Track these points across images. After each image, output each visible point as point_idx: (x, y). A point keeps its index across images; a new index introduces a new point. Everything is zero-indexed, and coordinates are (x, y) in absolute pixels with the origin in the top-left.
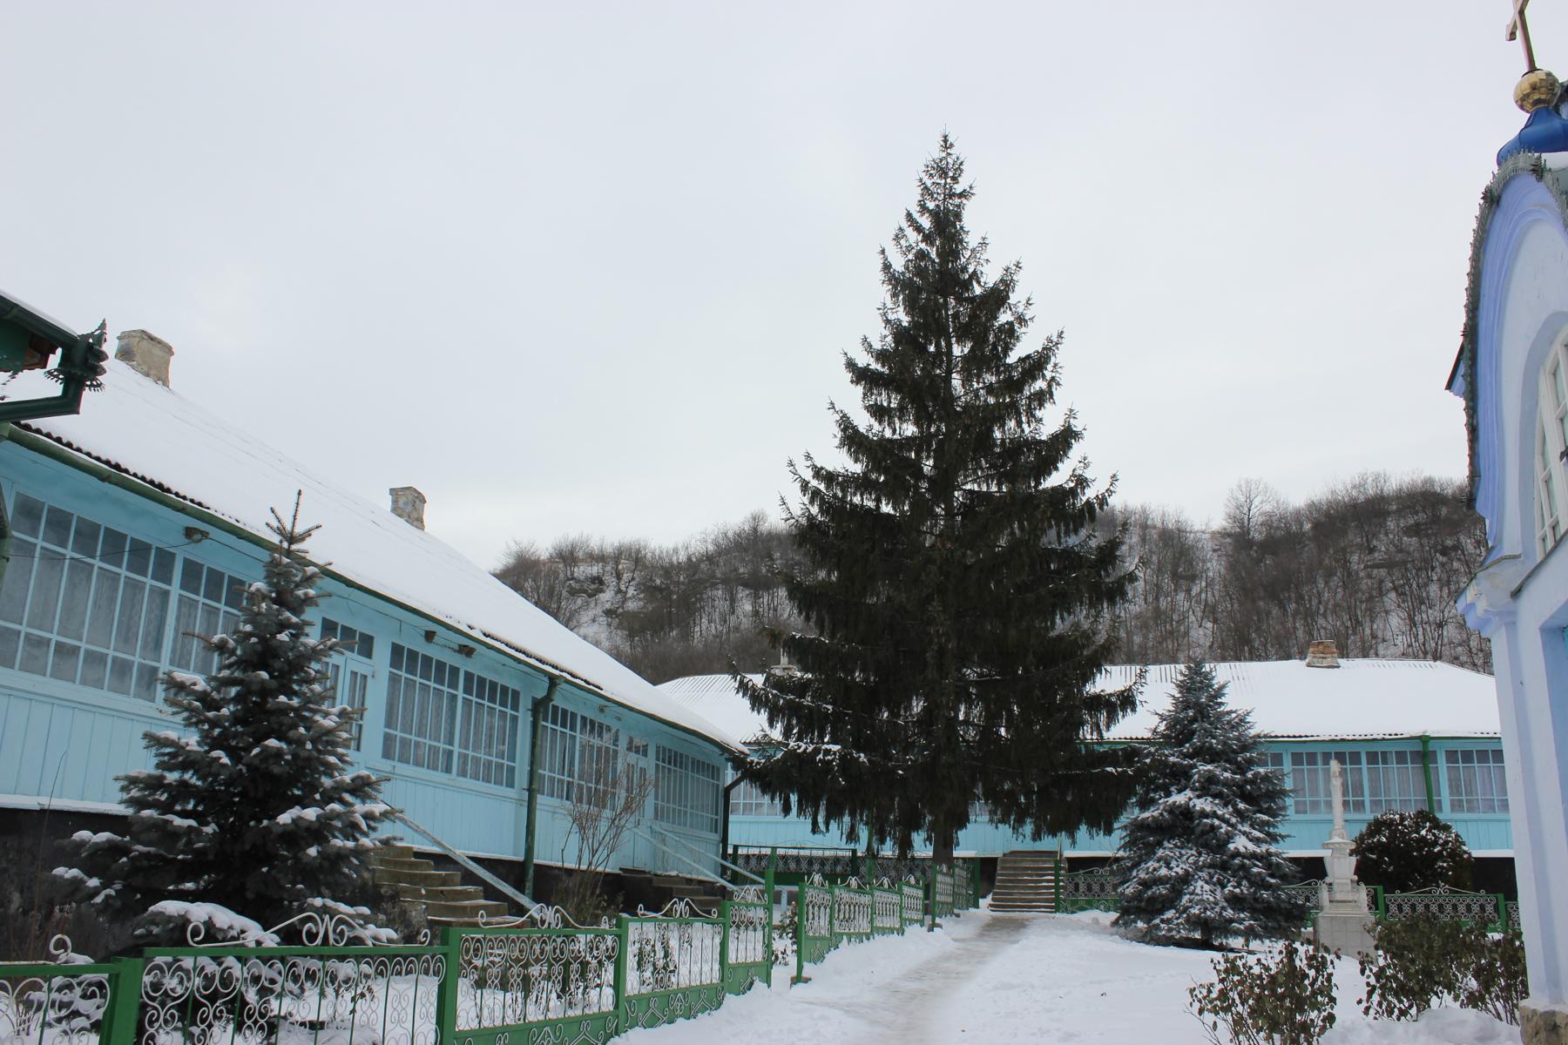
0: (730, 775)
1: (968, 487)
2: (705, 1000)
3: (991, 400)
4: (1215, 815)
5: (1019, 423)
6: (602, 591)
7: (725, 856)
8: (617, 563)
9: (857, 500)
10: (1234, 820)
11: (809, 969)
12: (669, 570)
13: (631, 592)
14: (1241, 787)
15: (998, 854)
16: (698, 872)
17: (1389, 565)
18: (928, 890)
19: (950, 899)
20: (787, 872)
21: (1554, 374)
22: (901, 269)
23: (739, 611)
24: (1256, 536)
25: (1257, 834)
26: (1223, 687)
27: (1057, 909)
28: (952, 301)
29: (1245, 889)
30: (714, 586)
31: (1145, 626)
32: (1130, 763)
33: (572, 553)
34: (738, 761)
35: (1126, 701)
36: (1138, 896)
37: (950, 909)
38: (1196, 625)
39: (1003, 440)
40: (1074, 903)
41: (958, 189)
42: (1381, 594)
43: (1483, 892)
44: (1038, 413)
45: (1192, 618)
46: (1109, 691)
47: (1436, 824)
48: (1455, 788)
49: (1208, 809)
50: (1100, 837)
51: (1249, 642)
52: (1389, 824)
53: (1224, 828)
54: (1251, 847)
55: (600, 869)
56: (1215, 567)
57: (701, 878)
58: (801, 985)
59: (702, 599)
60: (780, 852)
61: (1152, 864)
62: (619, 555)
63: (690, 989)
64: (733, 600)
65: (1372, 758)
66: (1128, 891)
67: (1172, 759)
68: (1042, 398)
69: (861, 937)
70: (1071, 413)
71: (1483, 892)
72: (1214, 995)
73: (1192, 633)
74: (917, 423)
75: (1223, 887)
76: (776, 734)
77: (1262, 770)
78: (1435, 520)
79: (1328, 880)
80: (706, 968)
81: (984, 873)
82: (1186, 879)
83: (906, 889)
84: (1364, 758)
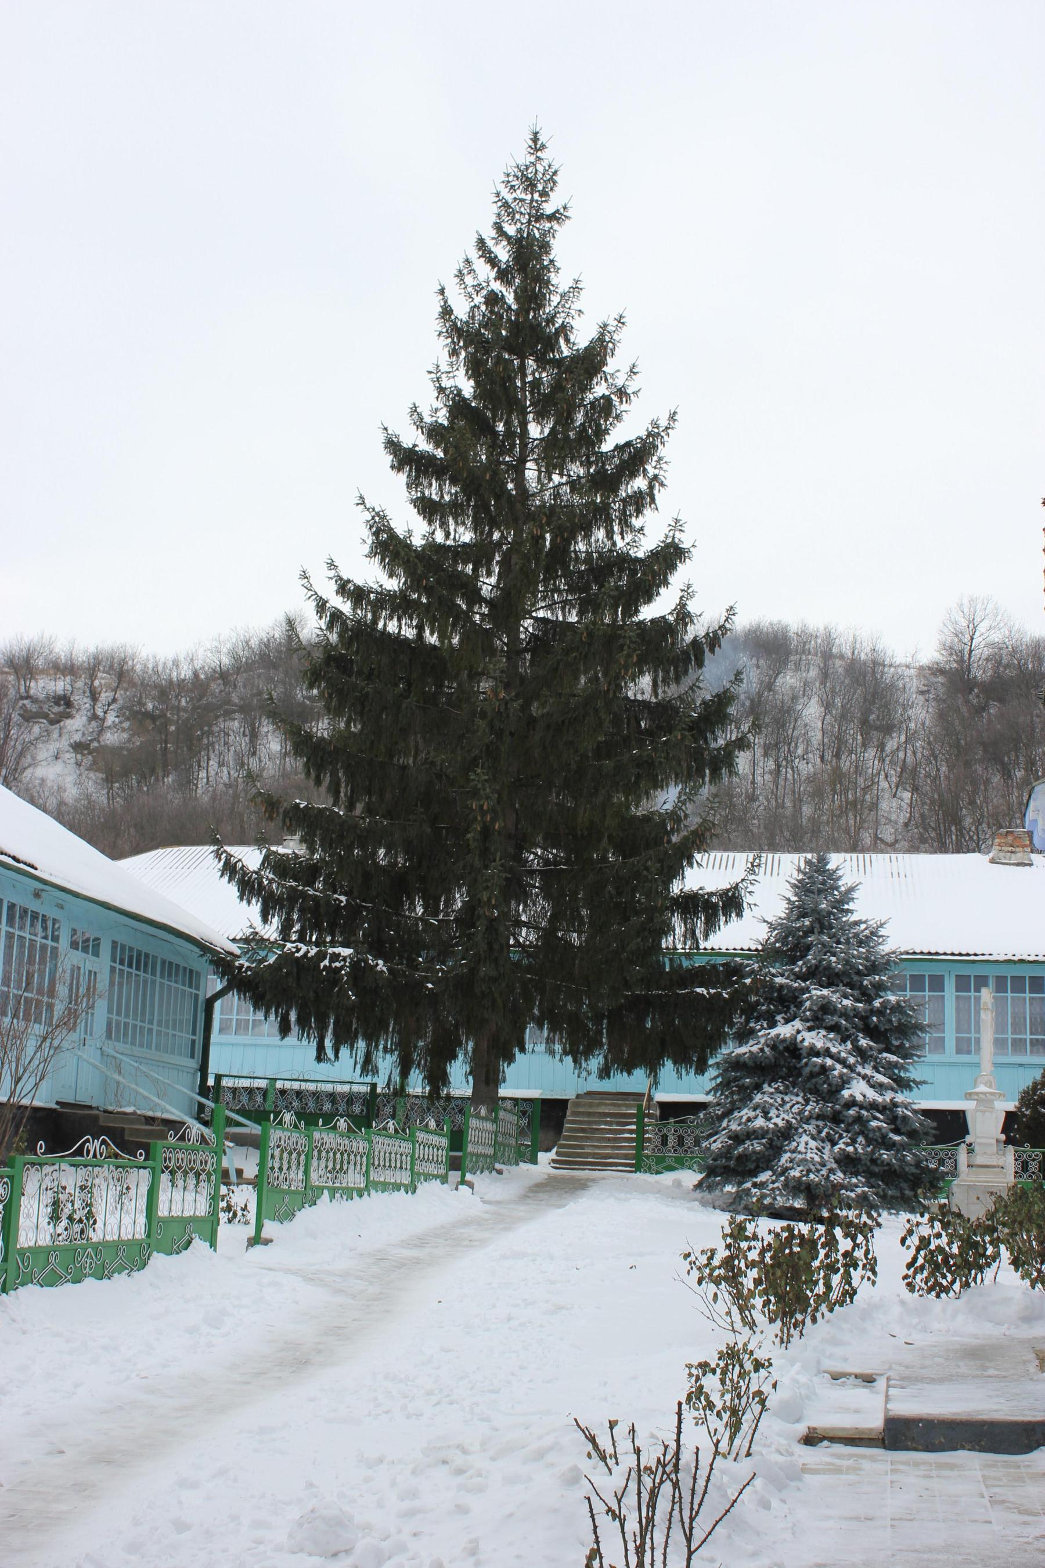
0: (215, 983)
1: (541, 614)
2: (131, 1257)
3: (576, 499)
4: (827, 1053)
5: (610, 534)
6: (69, 716)
7: (204, 1090)
8: (92, 677)
9: (392, 627)
10: (852, 1060)
11: (270, 1228)
12: (166, 689)
13: (111, 718)
14: (865, 1019)
15: (569, 1094)
16: (167, 1111)
18: (457, 1140)
19: (491, 1151)
20: (261, 1106)
22: (465, 318)
23: (262, 751)
24: (978, 673)
25: (881, 1078)
26: (852, 889)
27: (637, 1168)
28: (531, 363)
29: (861, 1147)
30: (228, 715)
31: (818, 794)
32: (726, 983)
33: (27, 660)
34: (223, 963)
35: (731, 902)
36: (726, 1153)
37: (489, 1164)
38: (887, 795)
39: (589, 554)
40: (660, 1160)
41: (548, 208)
44: (636, 522)
45: (884, 784)
46: (709, 889)
49: (819, 1045)
50: (691, 1078)
51: (957, 821)
54: (872, 1095)
55: (25, 1102)
56: (921, 714)
57: (166, 1116)
58: (258, 1248)
59: (210, 733)
60: (279, 1085)
61: (746, 1113)
62: (94, 667)
63: (104, 1244)
64: (254, 736)
65: (1001, 984)
66: (714, 1147)
67: (779, 980)
68: (640, 502)
69: (349, 1193)
70: (677, 525)
72: (716, 1262)
73: (884, 805)
74: (476, 527)
75: (834, 1143)
76: (271, 931)
77: (892, 998)
79: (968, 1139)
80: (127, 1220)
81: (548, 1117)
82: (787, 1133)
83: (421, 1136)
84: (991, 982)
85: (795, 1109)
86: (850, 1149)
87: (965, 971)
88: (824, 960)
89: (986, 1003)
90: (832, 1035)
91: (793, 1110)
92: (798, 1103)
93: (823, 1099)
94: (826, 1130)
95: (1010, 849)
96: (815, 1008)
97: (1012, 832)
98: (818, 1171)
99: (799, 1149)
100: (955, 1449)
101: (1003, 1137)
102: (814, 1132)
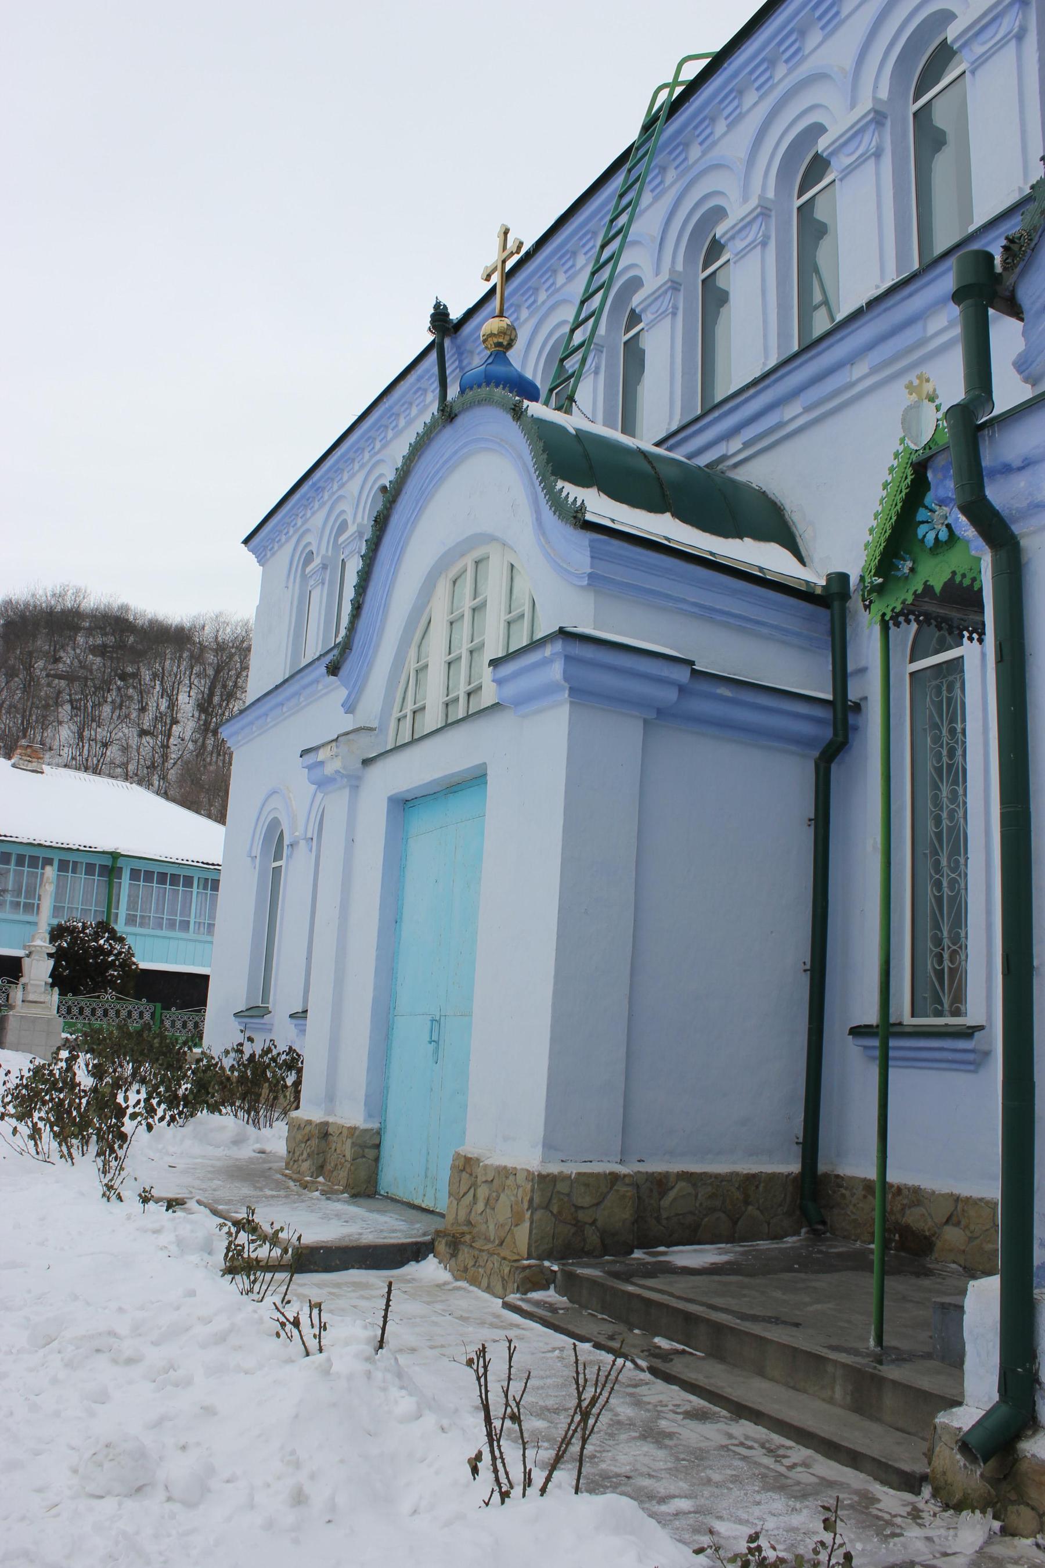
17: (69, 677)
21: (454, 582)
42: (57, 704)
43: (144, 1000)
47: (114, 936)
48: (132, 904)
52: (71, 930)
71: (144, 1000)
78: (121, 646)
79: (22, 980)
84: (56, 863)
87: (66, 856)
89: (48, 878)
100: (347, 1269)
101: (50, 980)
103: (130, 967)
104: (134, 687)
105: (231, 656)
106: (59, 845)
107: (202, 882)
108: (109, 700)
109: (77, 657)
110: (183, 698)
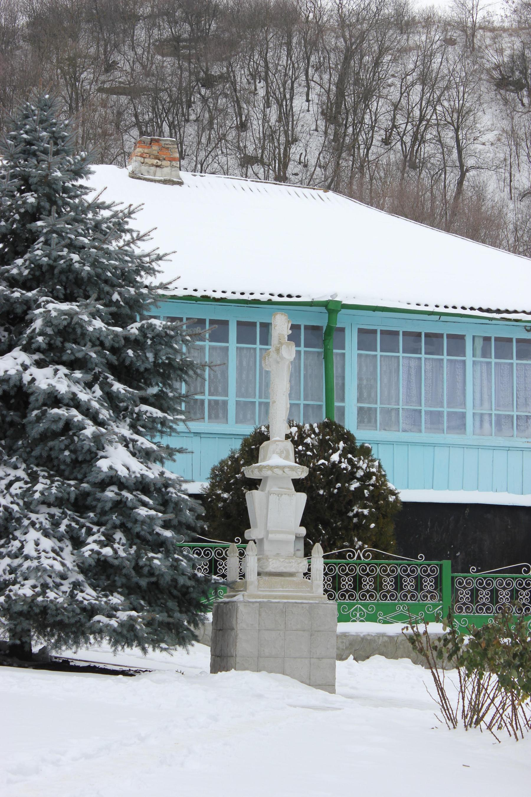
4: (74, 402)
17: (132, 91)
43: (421, 559)
49: (63, 387)
53: (90, 430)
54: (138, 467)
75: (78, 543)
78: (199, 37)
85: (16, 489)
86: (107, 551)
88: (61, 257)
90: (78, 374)
91: (13, 490)
92: (18, 479)
93: (60, 473)
94: (66, 522)
95: (155, 161)
96: (49, 331)
97: (157, 141)
98: (57, 586)
99: (26, 551)
101: (303, 531)
102: (47, 525)
103: (385, 499)
104: (226, 96)
105: (362, 37)
106: (238, 296)
107: (479, 343)
108: (193, 117)
109: (138, 59)
110: (299, 103)
